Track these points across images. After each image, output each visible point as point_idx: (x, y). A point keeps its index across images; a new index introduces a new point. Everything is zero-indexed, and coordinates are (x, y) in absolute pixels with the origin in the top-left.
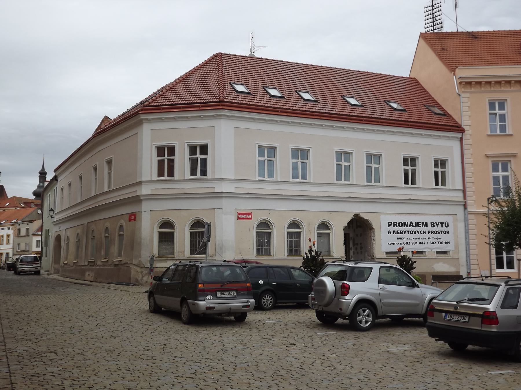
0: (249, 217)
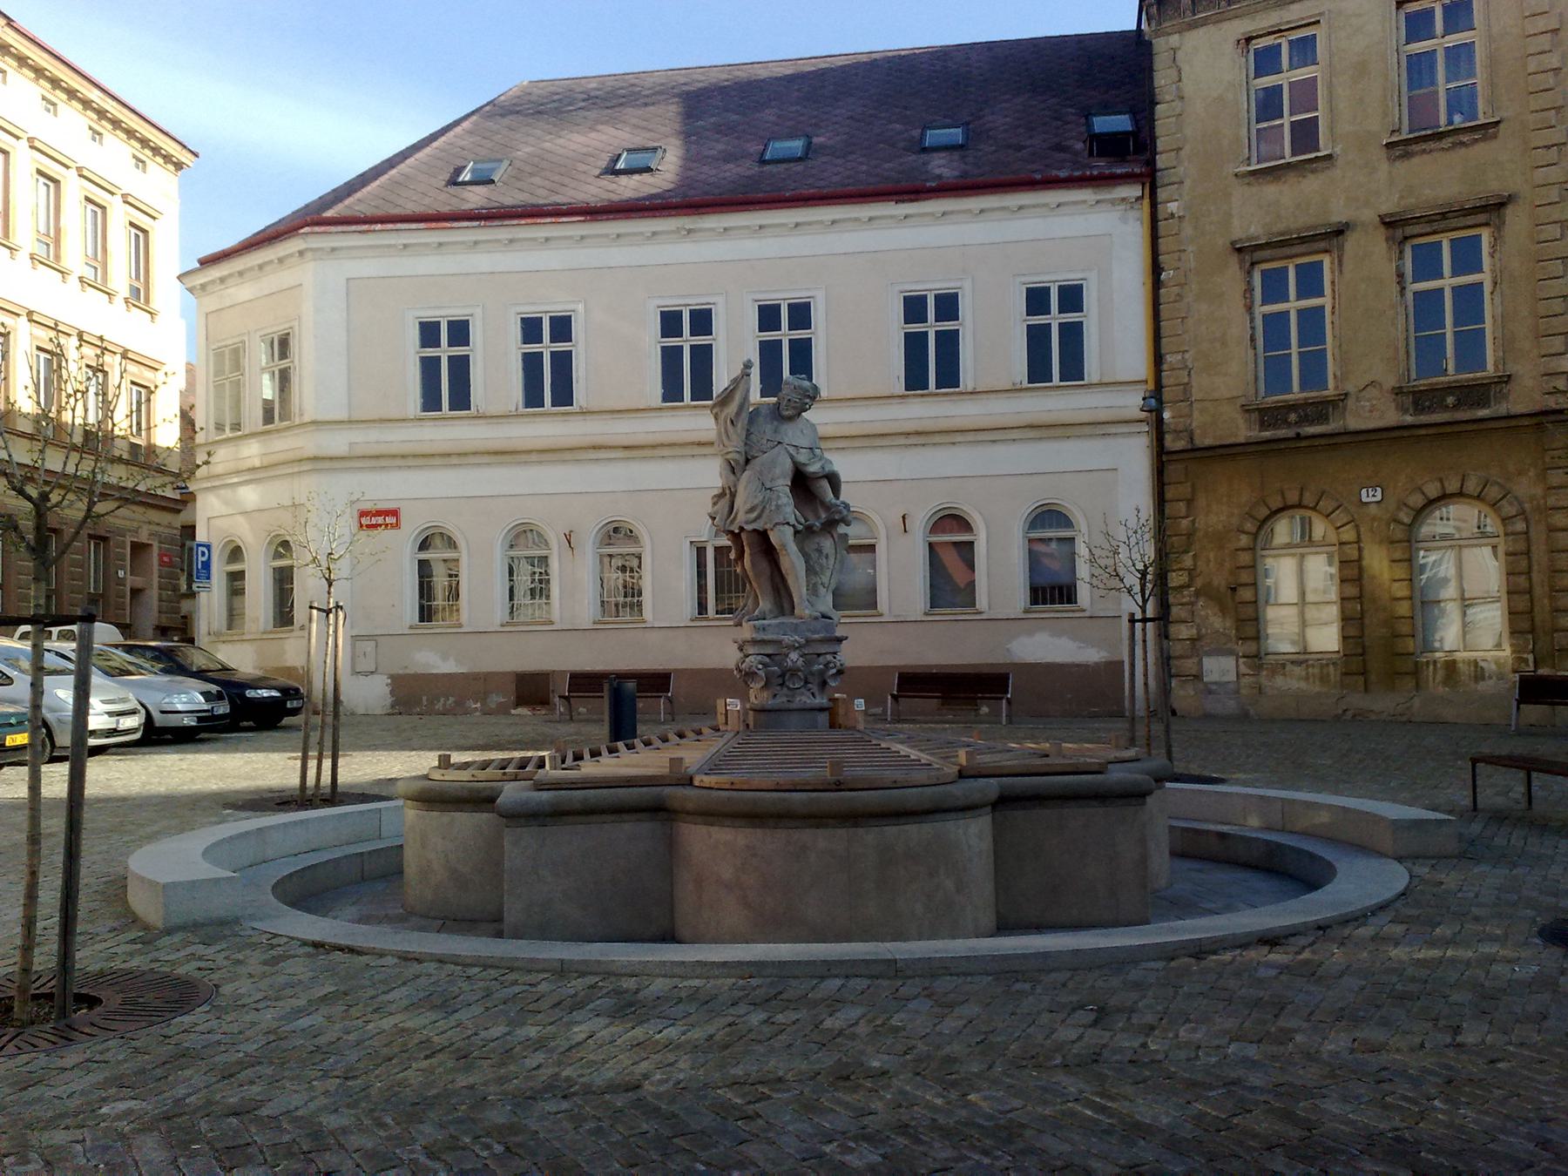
0: (390, 520)
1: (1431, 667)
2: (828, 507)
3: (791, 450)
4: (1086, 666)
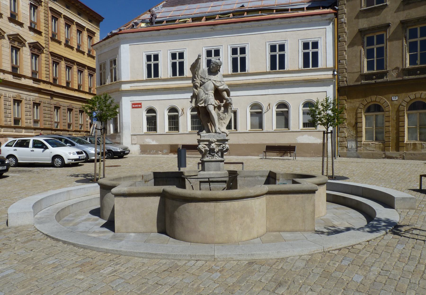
0: (140, 106)
1: (409, 145)
2: (227, 100)
3: (213, 82)
4: (317, 144)
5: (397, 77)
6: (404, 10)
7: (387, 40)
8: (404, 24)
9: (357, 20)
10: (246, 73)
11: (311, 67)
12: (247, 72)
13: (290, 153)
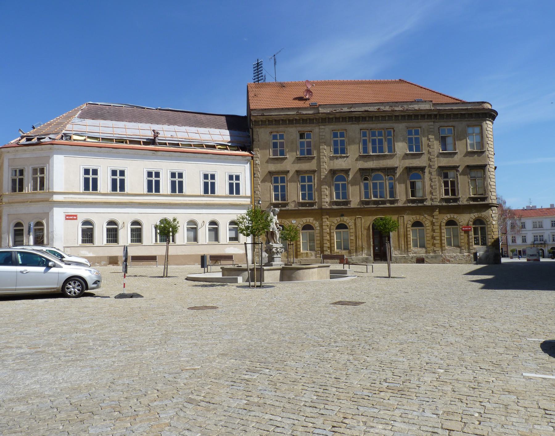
0: (75, 218)
5: (294, 207)
6: (297, 163)
7: (287, 181)
8: (298, 172)
9: (267, 164)
10: (183, 195)
11: (235, 195)
12: (184, 194)
13: (220, 260)
